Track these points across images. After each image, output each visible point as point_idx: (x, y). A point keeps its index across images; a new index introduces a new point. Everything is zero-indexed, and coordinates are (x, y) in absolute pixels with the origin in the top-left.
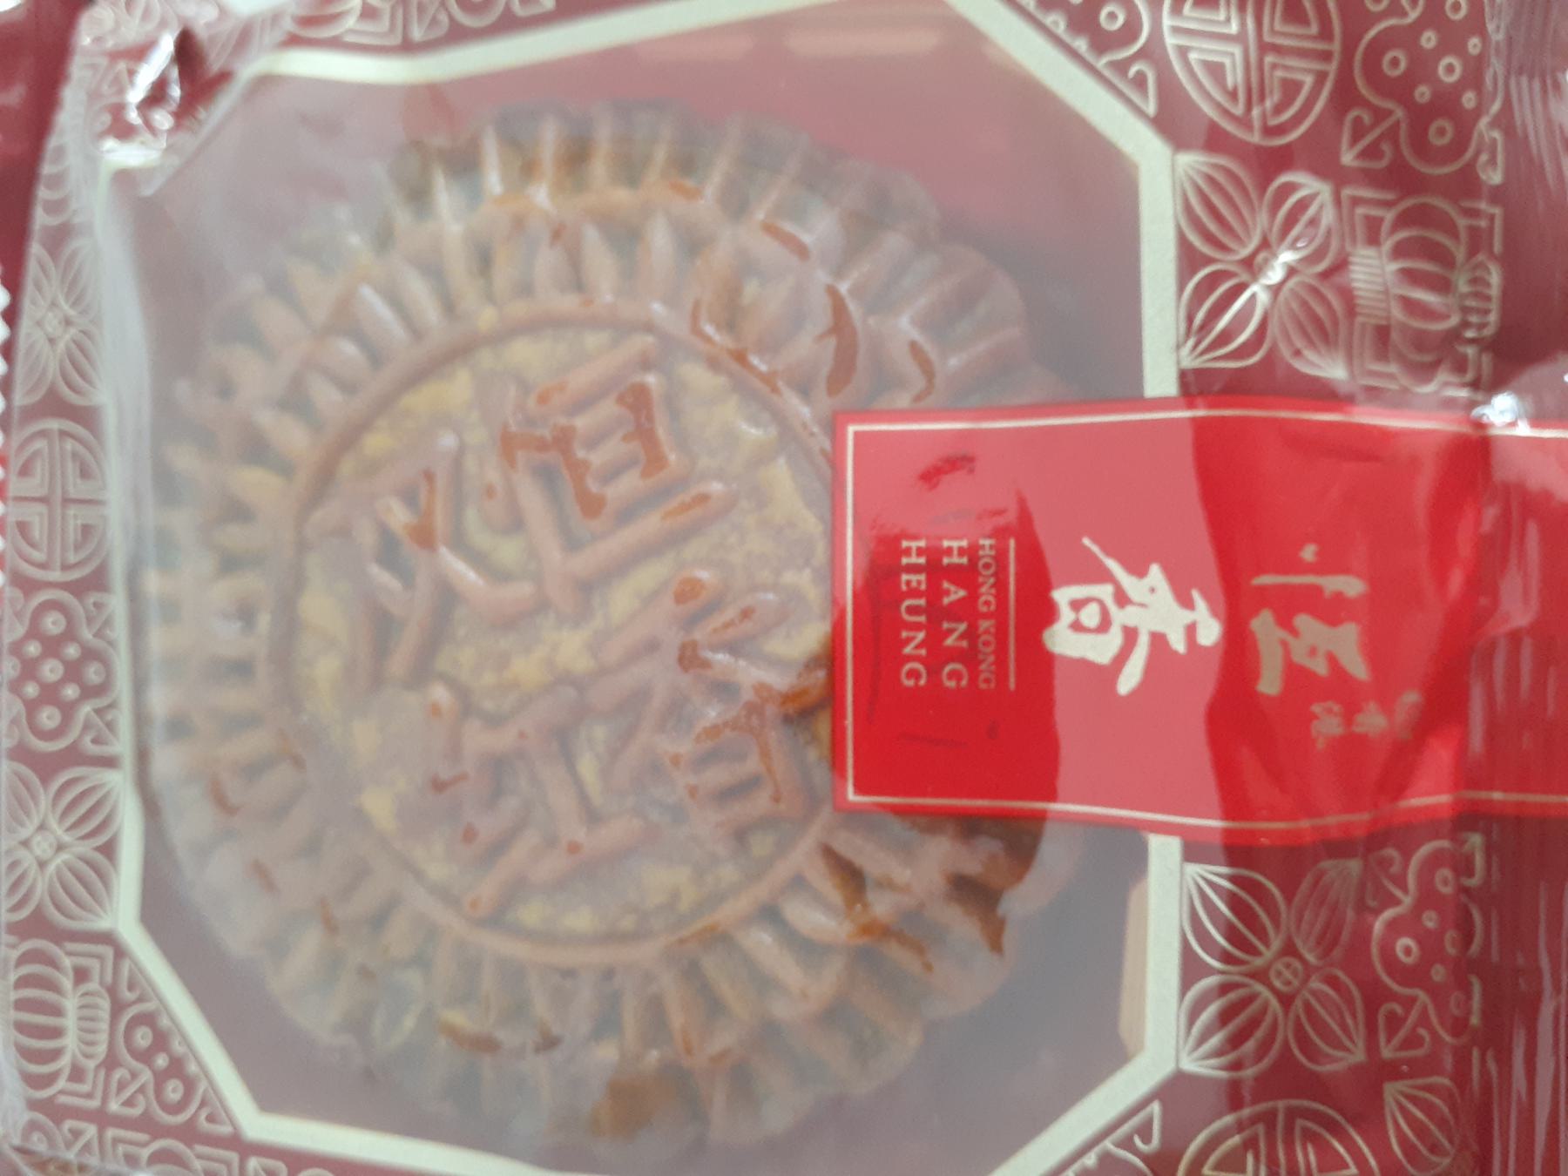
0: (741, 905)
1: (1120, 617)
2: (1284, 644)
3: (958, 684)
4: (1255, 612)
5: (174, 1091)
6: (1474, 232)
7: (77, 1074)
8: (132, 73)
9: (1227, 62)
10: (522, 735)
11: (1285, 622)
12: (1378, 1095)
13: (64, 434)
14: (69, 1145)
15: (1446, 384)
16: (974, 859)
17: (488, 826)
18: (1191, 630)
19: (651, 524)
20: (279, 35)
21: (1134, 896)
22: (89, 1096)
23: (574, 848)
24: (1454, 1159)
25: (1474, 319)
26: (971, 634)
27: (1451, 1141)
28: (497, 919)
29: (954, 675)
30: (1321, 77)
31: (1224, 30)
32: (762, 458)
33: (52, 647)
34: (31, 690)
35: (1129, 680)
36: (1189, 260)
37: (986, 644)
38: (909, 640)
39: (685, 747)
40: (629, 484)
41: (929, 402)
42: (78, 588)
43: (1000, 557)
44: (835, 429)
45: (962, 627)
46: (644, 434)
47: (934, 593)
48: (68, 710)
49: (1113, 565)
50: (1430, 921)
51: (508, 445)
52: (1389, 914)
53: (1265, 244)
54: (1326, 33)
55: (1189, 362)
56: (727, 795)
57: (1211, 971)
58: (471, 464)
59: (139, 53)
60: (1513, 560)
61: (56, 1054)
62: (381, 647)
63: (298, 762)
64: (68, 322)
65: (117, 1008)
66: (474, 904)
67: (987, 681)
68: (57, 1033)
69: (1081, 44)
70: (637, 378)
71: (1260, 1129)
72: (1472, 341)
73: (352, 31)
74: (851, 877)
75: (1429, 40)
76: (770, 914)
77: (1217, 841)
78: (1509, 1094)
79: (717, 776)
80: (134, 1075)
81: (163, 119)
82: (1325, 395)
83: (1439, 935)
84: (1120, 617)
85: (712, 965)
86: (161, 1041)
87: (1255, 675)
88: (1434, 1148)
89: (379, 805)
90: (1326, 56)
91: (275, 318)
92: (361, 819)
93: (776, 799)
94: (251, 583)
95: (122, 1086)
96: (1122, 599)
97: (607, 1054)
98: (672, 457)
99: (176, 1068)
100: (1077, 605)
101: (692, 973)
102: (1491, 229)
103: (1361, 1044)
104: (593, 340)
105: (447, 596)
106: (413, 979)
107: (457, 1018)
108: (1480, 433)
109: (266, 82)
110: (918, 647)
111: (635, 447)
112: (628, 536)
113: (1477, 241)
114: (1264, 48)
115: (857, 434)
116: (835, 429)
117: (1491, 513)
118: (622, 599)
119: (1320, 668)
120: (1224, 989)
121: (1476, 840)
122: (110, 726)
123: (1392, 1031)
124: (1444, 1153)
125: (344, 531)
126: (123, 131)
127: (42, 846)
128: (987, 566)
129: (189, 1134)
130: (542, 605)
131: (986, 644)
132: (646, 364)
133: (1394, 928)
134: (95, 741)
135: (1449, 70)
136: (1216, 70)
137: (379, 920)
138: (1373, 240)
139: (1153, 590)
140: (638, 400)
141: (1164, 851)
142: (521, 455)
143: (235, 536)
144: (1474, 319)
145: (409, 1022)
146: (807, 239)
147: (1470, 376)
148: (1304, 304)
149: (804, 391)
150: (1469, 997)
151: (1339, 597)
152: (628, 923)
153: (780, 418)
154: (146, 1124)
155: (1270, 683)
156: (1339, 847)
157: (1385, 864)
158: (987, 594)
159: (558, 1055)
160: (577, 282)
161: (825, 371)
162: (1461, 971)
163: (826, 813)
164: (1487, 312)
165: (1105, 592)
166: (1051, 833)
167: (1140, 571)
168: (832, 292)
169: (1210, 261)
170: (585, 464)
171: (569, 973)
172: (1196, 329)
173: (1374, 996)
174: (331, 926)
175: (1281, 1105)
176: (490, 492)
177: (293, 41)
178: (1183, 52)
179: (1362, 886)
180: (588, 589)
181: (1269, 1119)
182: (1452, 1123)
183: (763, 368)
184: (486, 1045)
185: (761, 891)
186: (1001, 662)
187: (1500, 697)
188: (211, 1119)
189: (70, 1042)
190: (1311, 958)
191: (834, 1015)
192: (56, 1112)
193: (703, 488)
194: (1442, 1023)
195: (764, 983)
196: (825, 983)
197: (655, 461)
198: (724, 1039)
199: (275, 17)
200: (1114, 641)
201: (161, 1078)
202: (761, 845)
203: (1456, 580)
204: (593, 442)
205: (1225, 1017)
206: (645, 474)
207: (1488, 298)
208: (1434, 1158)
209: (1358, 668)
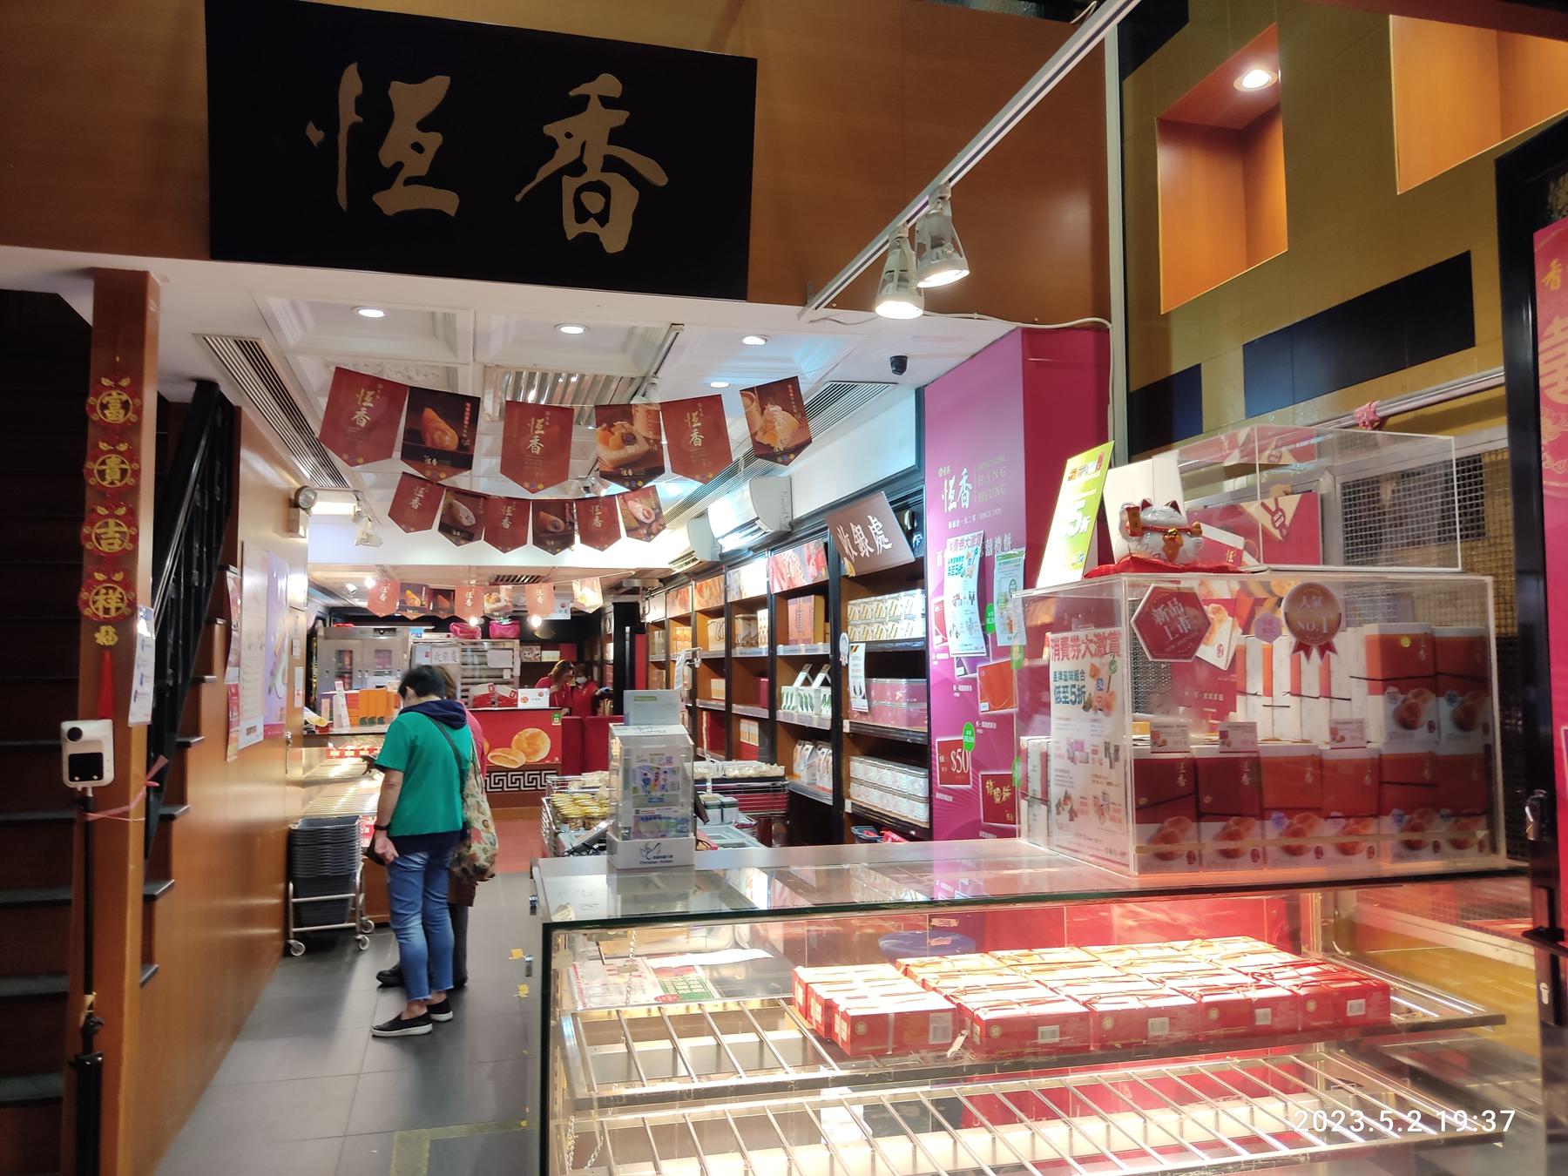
1: (593, 173)
11: (387, 177)
18: (607, 102)
35: (656, 174)
49: (544, 172)
84: (593, 173)
87: (439, 215)
96: (577, 168)
100: (582, 215)
101: (577, 804)
119: (433, 141)
139: (569, 135)
151: (361, 105)
165: (569, 185)
167: (551, 146)
200: (616, 181)
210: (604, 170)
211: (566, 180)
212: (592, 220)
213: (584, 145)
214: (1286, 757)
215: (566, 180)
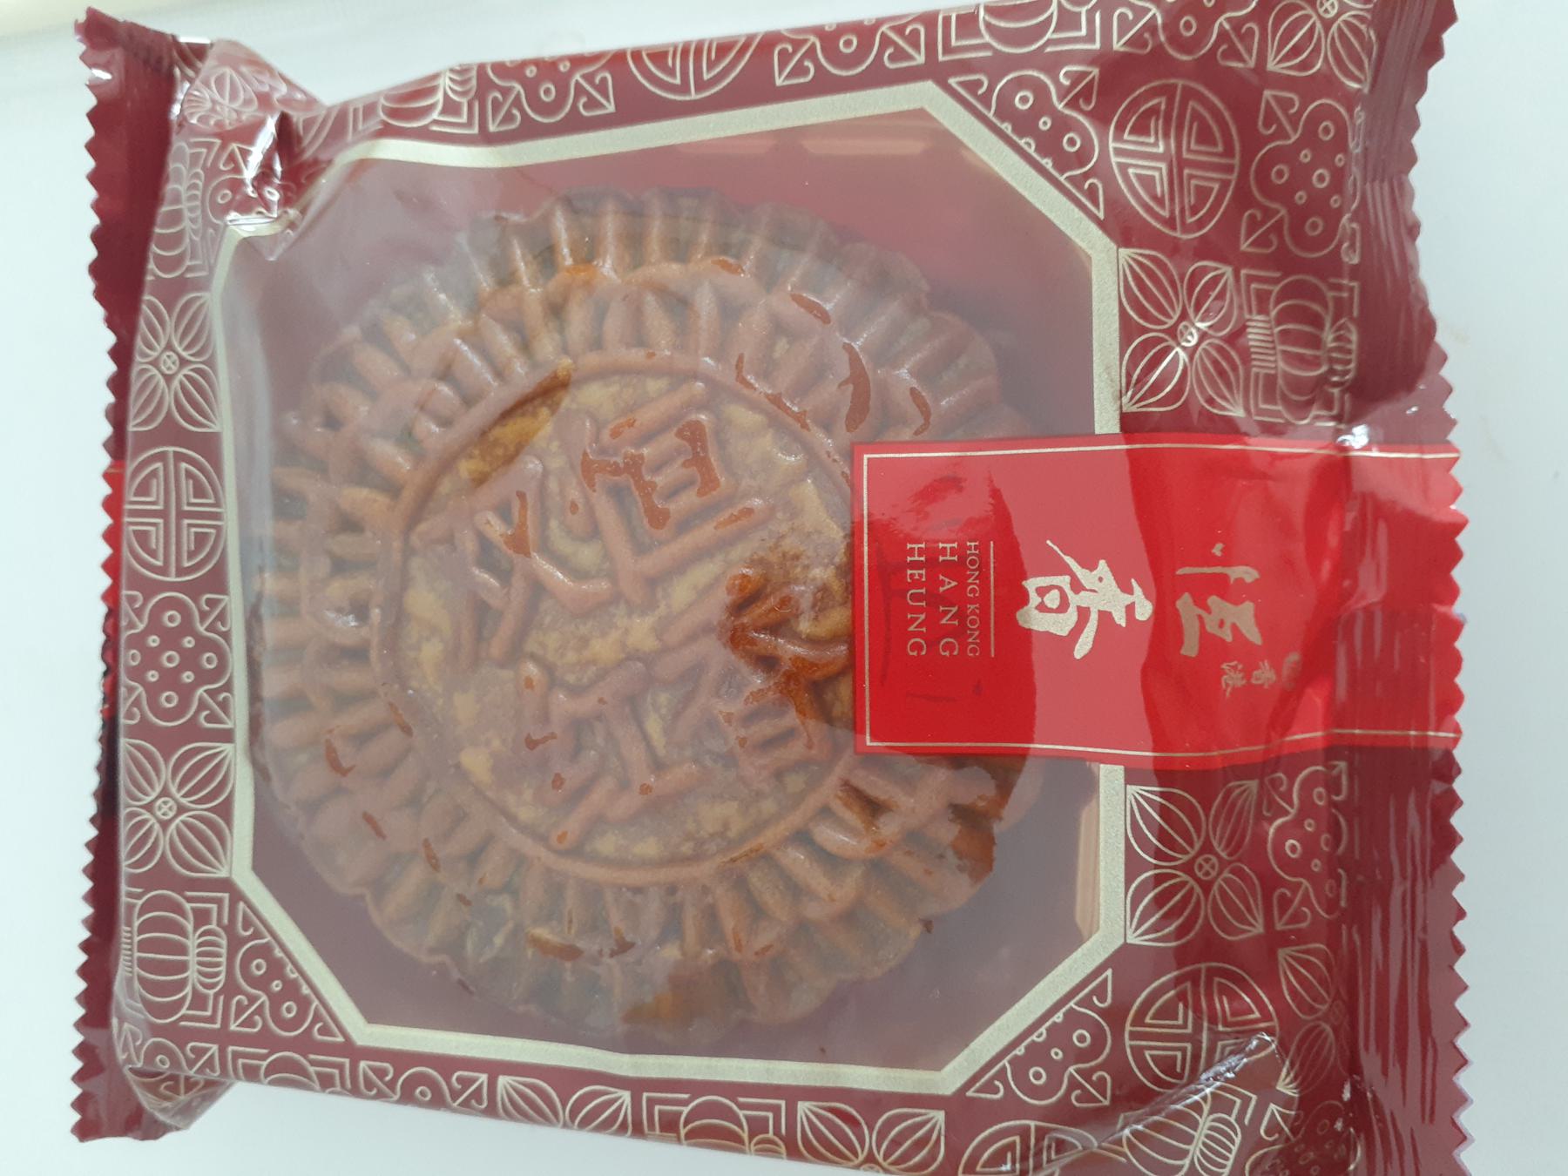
0: (782, 829)
1: (1075, 600)
2: (1200, 618)
3: (919, 653)
4: (1177, 596)
5: (289, 1010)
6: (1339, 302)
7: (199, 1001)
8: (245, 154)
9: (1156, 174)
10: (601, 701)
11: (1201, 602)
12: (1272, 955)
13: (179, 457)
14: (191, 1064)
15: (1317, 418)
16: (975, 787)
17: (573, 776)
18: (1130, 609)
19: (705, 532)
20: (374, 125)
21: (1085, 816)
22: (212, 1020)
23: (645, 789)
24: (1331, 1006)
25: (1338, 367)
26: (961, 615)
27: (1328, 992)
28: (576, 851)
29: (948, 647)
30: (1225, 185)
31: (1154, 150)
32: (796, 478)
33: (171, 639)
34: (153, 676)
35: (1082, 648)
36: (1128, 330)
37: (973, 622)
38: (913, 620)
39: (737, 707)
40: (688, 500)
41: (925, 436)
42: (193, 589)
43: (983, 556)
44: (852, 456)
45: (954, 609)
46: (699, 460)
47: (933, 582)
48: (186, 693)
49: (1069, 560)
50: (1309, 826)
51: (587, 471)
52: (1279, 821)
53: (1184, 316)
54: (1229, 152)
55: (1130, 408)
56: (769, 744)
57: (1147, 866)
58: (553, 485)
59: (248, 133)
60: (1368, 550)
61: (181, 985)
62: (479, 636)
63: (407, 730)
64: (183, 362)
65: (235, 943)
66: (561, 838)
67: (973, 650)
68: (183, 967)
69: (1047, 163)
70: (693, 417)
71: (1188, 985)
72: (1336, 385)
73: (436, 122)
74: (873, 808)
75: (1305, 156)
76: (802, 837)
77: (1150, 767)
78: (1370, 960)
79: (766, 728)
80: (252, 999)
81: (273, 195)
82: (1230, 429)
83: (1315, 837)
84: (1075, 600)
85: (756, 879)
86: (276, 969)
87: (1180, 642)
88: (1321, 1000)
89: (476, 762)
90: (1229, 169)
91: (376, 363)
92: (461, 773)
93: (809, 746)
94: (363, 583)
95: (241, 1009)
96: (1077, 586)
97: (671, 953)
98: (722, 480)
99: (291, 990)
100: (1042, 592)
101: (740, 884)
102: (1351, 298)
103: (1261, 920)
104: (654, 386)
105: (538, 588)
106: (505, 902)
107: (543, 932)
108: (1343, 454)
109: (362, 165)
110: (919, 626)
111: (693, 470)
112: (689, 541)
113: (1341, 309)
114: (1183, 164)
115: (869, 459)
116: (852, 456)
117: (1350, 516)
118: (681, 592)
120: (1159, 879)
121: (1342, 765)
122: (224, 706)
123: (1283, 911)
124: (1323, 1001)
125: (449, 540)
126: (245, 206)
127: (165, 809)
128: (973, 562)
129: (305, 1044)
130: (616, 598)
131: (973, 622)
132: (702, 407)
133: (1282, 833)
134: (209, 719)
135: (1321, 178)
136: (1147, 182)
137: (474, 858)
138: (1263, 310)
139: (1101, 579)
140: (694, 435)
141: (1110, 778)
142: (598, 478)
143: (345, 545)
144: (1338, 367)
145: (499, 940)
146: (828, 307)
147: (1335, 412)
148: (1215, 363)
149: (828, 428)
150: (1339, 885)
152: (687, 848)
153: (809, 451)
154: (265, 1039)
155: (1190, 648)
156: (1244, 770)
157: (1275, 784)
158: (973, 583)
159: (630, 957)
160: (638, 337)
161: (845, 411)
162: (1332, 863)
163: (848, 757)
164: (1348, 362)
165: (1064, 581)
166: (1030, 765)
167: (1090, 566)
168: (849, 349)
169: (1145, 330)
170: (653, 485)
171: (638, 890)
172: (1132, 382)
173: (1270, 883)
174: (433, 863)
175: (1203, 966)
176: (574, 507)
177: (387, 132)
178: (1123, 168)
179: (1259, 805)
180: (653, 583)
181: (1194, 978)
182: (1329, 980)
183: (795, 409)
184: (571, 953)
185: (795, 819)
186: (984, 636)
187: (1359, 658)
188: (325, 1031)
189: (192, 974)
190: (1224, 855)
191: (850, 917)
192: (180, 1035)
193: (748, 504)
194: (1319, 903)
195: (796, 890)
196: (847, 889)
197: (709, 483)
198: (765, 937)
199: (369, 110)
200: (1071, 617)
201: (276, 1001)
202: (795, 782)
203: (1326, 567)
204: (658, 468)
205: (1159, 901)
206: (700, 493)
207: (1349, 352)
208: (1317, 1006)
209: (1254, 635)
210: (1079, 609)
211: (1067, 578)
212: (1039, 600)
213: (1094, 591)
214: (220, 1095)
215: (1067, 578)
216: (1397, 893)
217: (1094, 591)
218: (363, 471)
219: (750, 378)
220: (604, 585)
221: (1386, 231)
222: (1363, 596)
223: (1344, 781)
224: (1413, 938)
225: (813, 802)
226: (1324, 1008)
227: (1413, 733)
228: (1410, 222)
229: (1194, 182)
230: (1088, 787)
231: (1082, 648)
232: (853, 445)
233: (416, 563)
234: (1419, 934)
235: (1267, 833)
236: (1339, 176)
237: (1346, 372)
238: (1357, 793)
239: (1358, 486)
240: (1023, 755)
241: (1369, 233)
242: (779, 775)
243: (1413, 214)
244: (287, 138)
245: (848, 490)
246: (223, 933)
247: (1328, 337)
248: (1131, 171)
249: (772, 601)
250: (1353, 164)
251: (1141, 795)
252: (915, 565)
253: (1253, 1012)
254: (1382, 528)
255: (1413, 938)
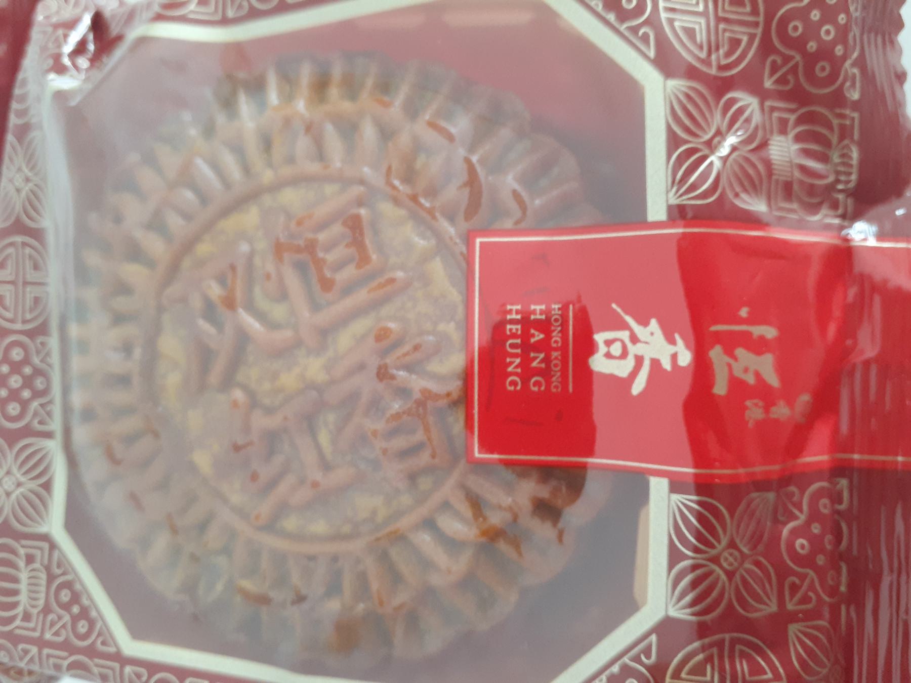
1: (633, 350)
2: (729, 366)
5: (83, 626)
6: (842, 128)
7: (27, 617)
8: (66, 36)
10: (285, 418)
13: (24, 244)
14: (21, 659)
15: (826, 216)
17: (266, 472)
18: (674, 357)
19: (362, 296)
20: (151, 14)
22: (34, 630)
23: (315, 485)
25: (843, 178)
26: (547, 360)
27: (829, 660)
28: (271, 526)
29: (537, 383)
30: (752, 37)
31: (696, 9)
35: (638, 386)
36: (673, 141)
37: (556, 366)
38: (511, 363)
39: (380, 426)
40: (349, 273)
41: (523, 225)
42: (31, 334)
45: (542, 356)
46: (358, 242)
47: (526, 336)
48: (24, 404)
49: (629, 319)
50: (816, 529)
51: (279, 249)
52: (792, 525)
57: (686, 557)
58: (257, 261)
59: (71, 25)
61: (14, 605)
63: (156, 435)
65: (51, 578)
66: (257, 517)
67: (556, 387)
69: (611, 17)
71: (715, 650)
75: (815, 15)
76: (429, 524)
77: (691, 480)
79: (400, 443)
83: (821, 538)
84: (633, 350)
85: (395, 553)
86: (76, 598)
89: (203, 460)
92: (193, 468)
94: (130, 330)
96: (634, 339)
97: (334, 606)
98: (374, 257)
99: (84, 613)
100: (608, 343)
101: (384, 558)
103: (774, 600)
104: (329, 189)
105: (243, 338)
106: (221, 561)
109: (143, 41)
110: (516, 367)
111: (352, 251)
112: (348, 303)
115: (481, 243)
117: (852, 292)
118: (344, 340)
119: (751, 379)
120: (694, 568)
121: (844, 483)
122: (49, 414)
126: (60, 69)
128: (556, 320)
129: (91, 652)
130: (298, 343)
131: (556, 366)
132: (360, 203)
133: (795, 533)
134: (40, 423)
135: (828, 33)
136: (690, 33)
137: (203, 527)
138: (783, 131)
139: (652, 334)
141: (658, 487)
143: (121, 303)
146: (453, 130)
147: (840, 211)
149: (451, 219)
151: (762, 338)
152: (347, 529)
153: (438, 235)
154: (66, 646)
155: (720, 388)
156: (762, 485)
158: (556, 337)
159: (305, 606)
160: (320, 155)
162: (836, 559)
163: (462, 464)
164: (850, 174)
165: (624, 335)
167: (645, 323)
168: (468, 161)
170: (324, 261)
171: (312, 558)
174: (174, 530)
176: (268, 277)
177: (159, 18)
178: (671, 21)
179: (775, 512)
180: (325, 333)
181: (720, 644)
184: (263, 600)
185: (424, 511)
186: (564, 375)
189: (23, 598)
190: (745, 550)
193: (391, 275)
195: (427, 564)
197: (364, 259)
198: (402, 597)
201: (75, 619)
202: (425, 483)
203: (832, 330)
204: (328, 248)
205: (694, 584)
206: (359, 266)
209: (773, 380)
213: (646, 343)
216: (887, 580)
217: (646, 343)
218: (135, 253)
219: (397, 183)
220: (288, 334)
221: (881, 78)
222: (862, 352)
223: (846, 495)
224: (897, 619)
225: (437, 498)
226: (825, 671)
227: (900, 459)
228: (899, 70)
229: (727, 34)
230: (642, 496)
231: (638, 386)
232: (469, 232)
233: (166, 318)
234: (902, 615)
235: (781, 532)
236: (843, 33)
237: (848, 182)
238: (855, 502)
239: (857, 269)
240: (584, 467)
241: (868, 77)
242: (412, 477)
243: (901, 66)
244: (98, 24)
245: (464, 265)
246: (44, 571)
247: (836, 158)
248: (677, 24)
249: (407, 348)
250: (853, 23)
251: (682, 503)
252: (512, 322)
253: (765, 673)
254: (877, 300)
255: (897, 619)
